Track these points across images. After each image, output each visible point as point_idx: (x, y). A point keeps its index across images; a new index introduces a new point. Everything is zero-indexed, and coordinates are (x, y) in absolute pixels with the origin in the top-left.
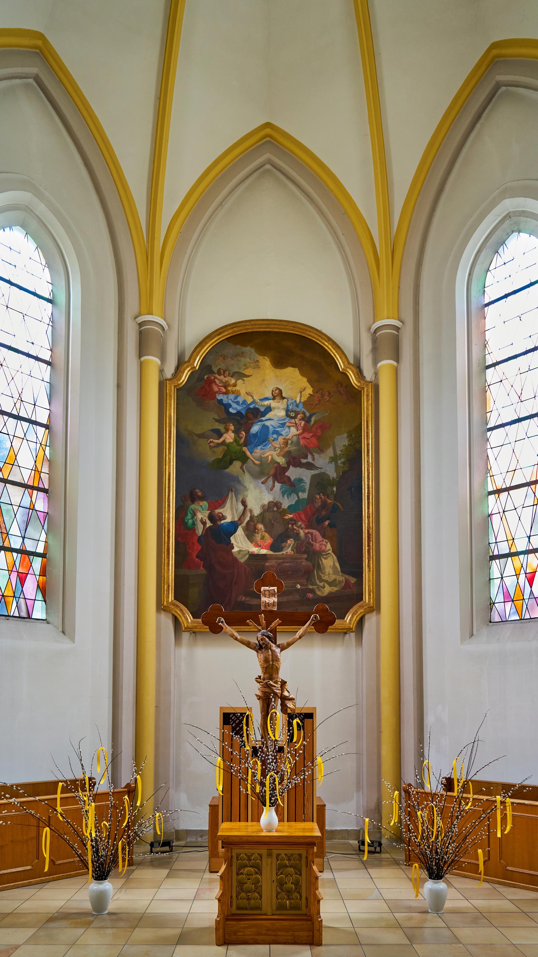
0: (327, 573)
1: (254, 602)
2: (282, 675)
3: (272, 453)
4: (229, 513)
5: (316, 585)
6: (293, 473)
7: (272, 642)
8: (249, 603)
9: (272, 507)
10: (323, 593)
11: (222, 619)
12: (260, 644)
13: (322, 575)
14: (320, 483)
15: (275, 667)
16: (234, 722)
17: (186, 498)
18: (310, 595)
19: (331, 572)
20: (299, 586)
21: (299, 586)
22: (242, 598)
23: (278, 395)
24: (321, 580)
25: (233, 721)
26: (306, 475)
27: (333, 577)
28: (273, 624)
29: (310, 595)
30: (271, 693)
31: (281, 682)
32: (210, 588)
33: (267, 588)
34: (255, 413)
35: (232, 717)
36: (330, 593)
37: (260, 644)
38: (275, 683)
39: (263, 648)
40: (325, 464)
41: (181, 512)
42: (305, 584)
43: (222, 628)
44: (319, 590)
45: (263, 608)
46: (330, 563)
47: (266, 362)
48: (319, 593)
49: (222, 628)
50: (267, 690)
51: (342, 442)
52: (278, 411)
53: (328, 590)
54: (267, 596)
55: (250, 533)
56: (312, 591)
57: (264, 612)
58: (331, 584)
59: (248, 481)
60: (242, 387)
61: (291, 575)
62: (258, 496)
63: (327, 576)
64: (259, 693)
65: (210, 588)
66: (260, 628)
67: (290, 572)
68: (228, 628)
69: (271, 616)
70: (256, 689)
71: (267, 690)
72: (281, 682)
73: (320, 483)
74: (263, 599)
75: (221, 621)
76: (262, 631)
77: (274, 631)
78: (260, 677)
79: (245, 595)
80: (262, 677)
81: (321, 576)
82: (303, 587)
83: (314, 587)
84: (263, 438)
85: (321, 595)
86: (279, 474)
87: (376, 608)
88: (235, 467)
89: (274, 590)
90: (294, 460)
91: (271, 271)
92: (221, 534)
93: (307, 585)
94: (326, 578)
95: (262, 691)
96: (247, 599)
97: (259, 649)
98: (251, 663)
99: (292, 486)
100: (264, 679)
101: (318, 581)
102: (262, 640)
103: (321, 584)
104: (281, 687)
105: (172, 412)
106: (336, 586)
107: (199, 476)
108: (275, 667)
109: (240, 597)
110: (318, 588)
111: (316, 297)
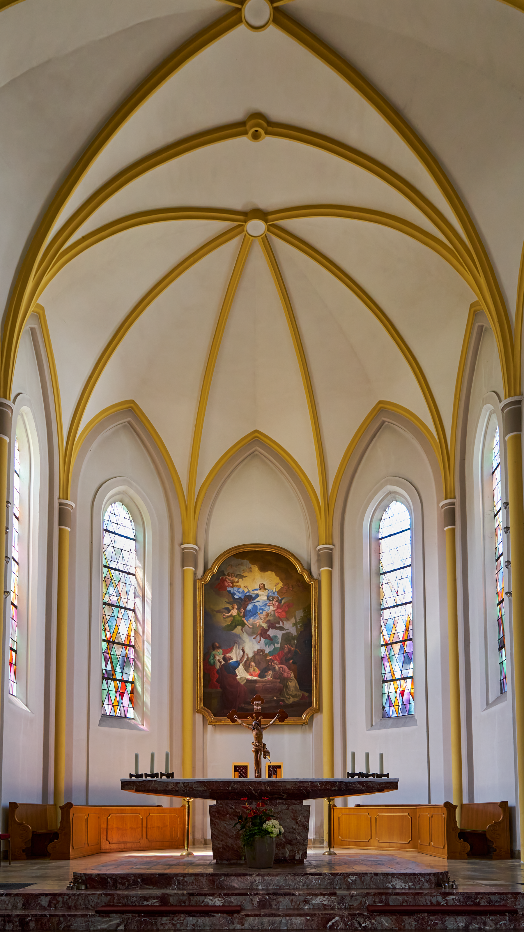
3: (259, 621)
4: (234, 656)
6: (271, 633)
9: (261, 651)
14: (287, 638)
17: (210, 647)
20: (275, 698)
23: (263, 587)
24: (288, 694)
26: (279, 634)
27: (295, 693)
29: (282, 703)
32: (222, 697)
34: (250, 598)
36: (294, 702)
40: (290, 627)
41: (207, 655)
46: (293, 684)
47: (255, 569)
48: (287, 702)
49: (236, 720)
50: (257, 747)
51: (299, 614)
52: (263, 597)
53: (292, 700)
55: (247, 667)
56: (283, 701)
57: (255, 713)
58: (294, 697)
59: (245, 637)
60: (242, 583)
62: (251, 646)
64: (254, 749)
65: (222, 697)
68: (239, 721)
69: (258, 714)
71: (257, 747)
73: (287, 638)
74: (255, 707)
75: (235, 717)
77: (260, 721)
84: (254, 612)
86: (263, 633)
87: (319, 710)
88: (238, 630)
90: (272, 625)
91: (254, 515)
92: (230, 669)
94: (290, 693)
98: (250, 737)
99: (271, 640)
103: (288, 697)
105: (201, 598)
106: (296, 698)
107: (214, 636)
111: (285, 528)
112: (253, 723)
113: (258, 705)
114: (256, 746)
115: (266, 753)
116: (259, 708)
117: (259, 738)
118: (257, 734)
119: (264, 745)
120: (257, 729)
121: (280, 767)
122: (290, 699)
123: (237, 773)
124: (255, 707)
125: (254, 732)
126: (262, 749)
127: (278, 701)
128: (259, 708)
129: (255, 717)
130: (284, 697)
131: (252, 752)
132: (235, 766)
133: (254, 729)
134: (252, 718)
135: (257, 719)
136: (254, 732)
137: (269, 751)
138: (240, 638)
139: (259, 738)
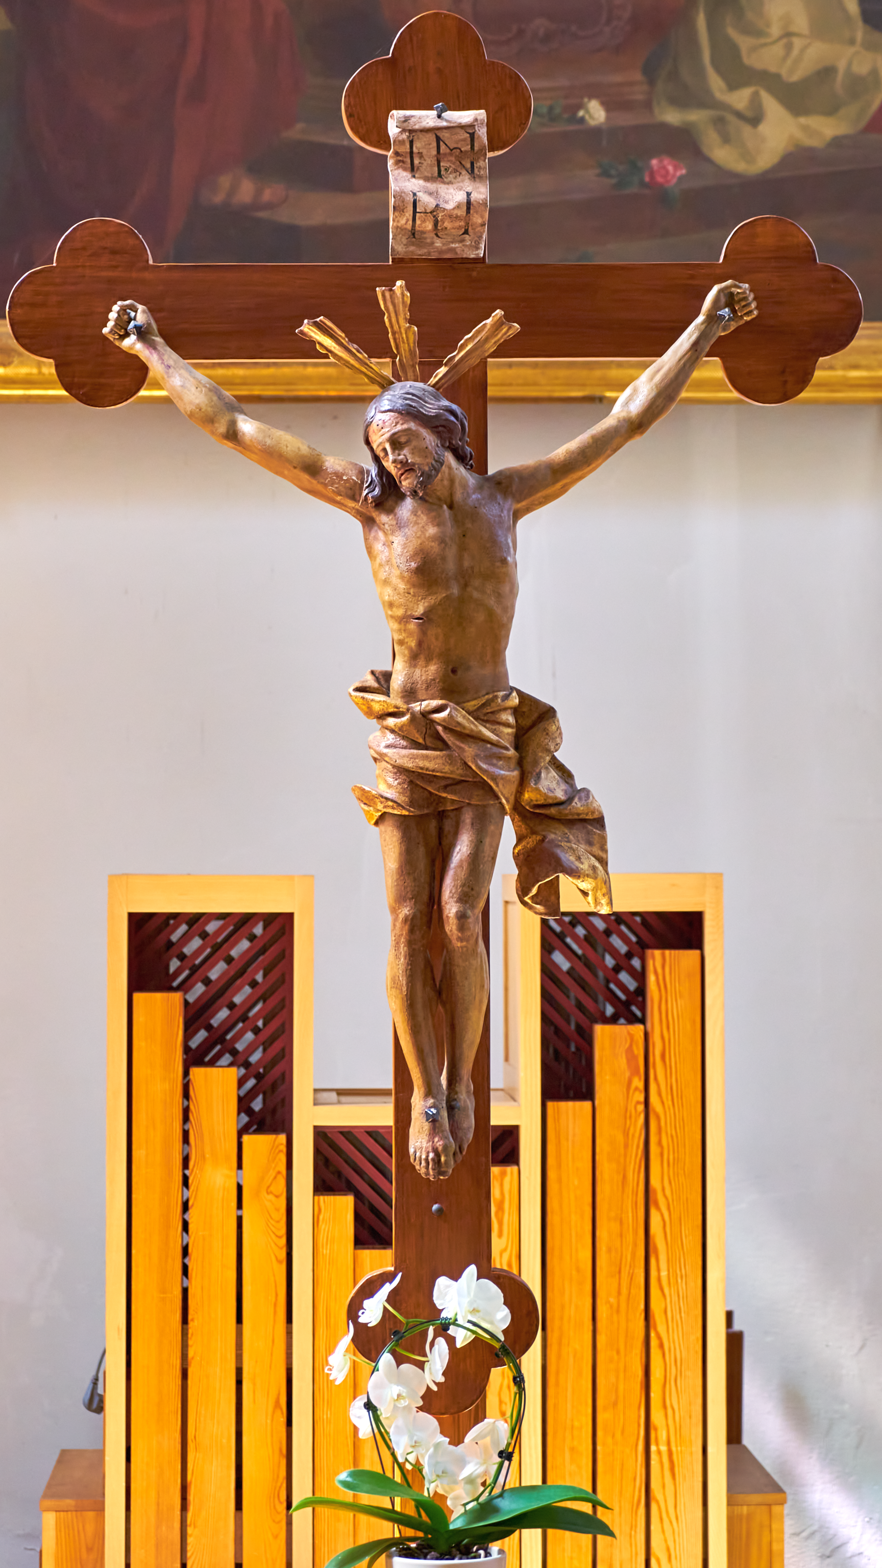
0: (775, 31)
1: (317, 209)
2: (527, 665)
5: (705, 101)
7: (461, 458)
8: (284, 216)
10: (747, 156)
11: (141, 316)
12: (382, 471)
13: (744, 42)
15: (480, 617)
16: (196, 971)
18: (670, 171)
19: (801, 23)
20: (596, 113)
21: (596, 113)
22: (233, 190)
24: (738, 74)
25: (211, 980)
27: (811, 55)
28: (468, 343)
29: (670, 171)
30: (477, 775)
31: (516, 711)
33: (427, 118)
35: (186, 938)
36: (797, 157)
37: (382, 471)
38: (480, 715)
39: (401, 497)
42: (638, 94)
43: (143, 369)
44: (726, 139)
45: (396, 244)
48: (723, 155)
49: (138, 372)
50: (429, 760)
53: (777, 135)
54: (428, 164)
56: (683, 143)
57: (403, 266)
58: (798, 98)
61: (548, 38)
63: (778, 50)
64: (388, 787)
66: (383, 367)
67: (540, 25)
68: (178, 379)
69: (452, 289)
70: (373, 758)
71: (429, 760)
72: (516, 711)
74: (401, 182)
75: (126, 324)
76: (400, 389)
77: (470, 389)
78: (384, 679)
79: (258, 169)
80: (397, 682)
81: (735, 50)
82: (627, 119)
83: (695, 116)
85: (740, 167)
89: (469, 129)
93: (648, 105)
94: (767, 58)
95: (400, 770)
96: (267, 195)
97: (380, 504)
98: (352, 584)
100: (410, 694)
101: (716, 83)
102: (396, 442)
103: (740, 99)
104: (520, 741)
106: (831, 110)
108: (480, 617)
109: (225, 181)
110: (719, 123)
112: (382, 419)
113: (448, 156)
114: (424, 733)
115: (561, 828)
116: (453, 195)
117: (460, 607)
118: (425, 572)
119: (535, 720)
120: (425, 496)
121: (683, 930)
122: (755, 118)
123: (162, 1010)
124: (401, 182)
125: (405, 533)
126: (504, 776)
127: (633, 144)
128: (453, 195)
129: (402, 331)
130: (700, 98)
131: (361, 818)
132: (139, 923)
133: (389, 493)
134: (370, 337)
135: (435, 343)
136: (405, 533)
137: (604, 800)
138: (400, 793)
139: (460, 607)
